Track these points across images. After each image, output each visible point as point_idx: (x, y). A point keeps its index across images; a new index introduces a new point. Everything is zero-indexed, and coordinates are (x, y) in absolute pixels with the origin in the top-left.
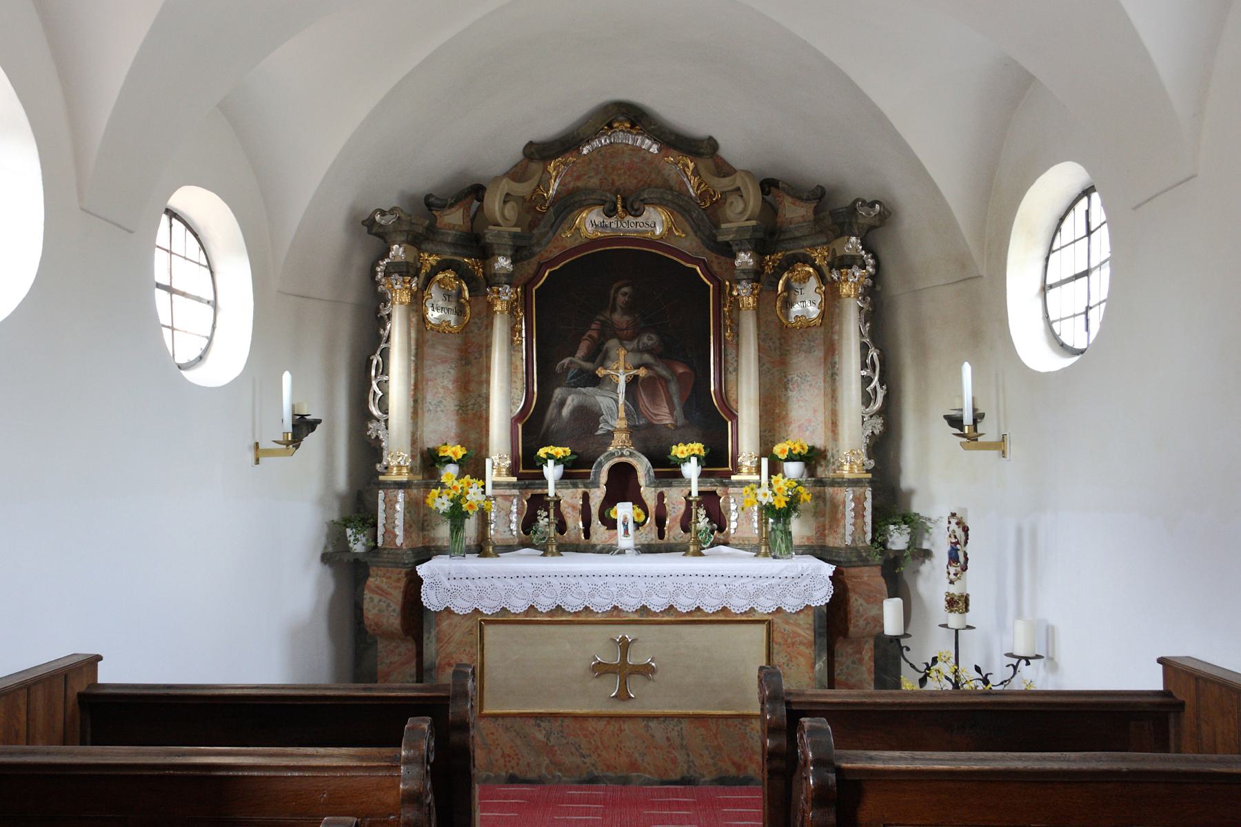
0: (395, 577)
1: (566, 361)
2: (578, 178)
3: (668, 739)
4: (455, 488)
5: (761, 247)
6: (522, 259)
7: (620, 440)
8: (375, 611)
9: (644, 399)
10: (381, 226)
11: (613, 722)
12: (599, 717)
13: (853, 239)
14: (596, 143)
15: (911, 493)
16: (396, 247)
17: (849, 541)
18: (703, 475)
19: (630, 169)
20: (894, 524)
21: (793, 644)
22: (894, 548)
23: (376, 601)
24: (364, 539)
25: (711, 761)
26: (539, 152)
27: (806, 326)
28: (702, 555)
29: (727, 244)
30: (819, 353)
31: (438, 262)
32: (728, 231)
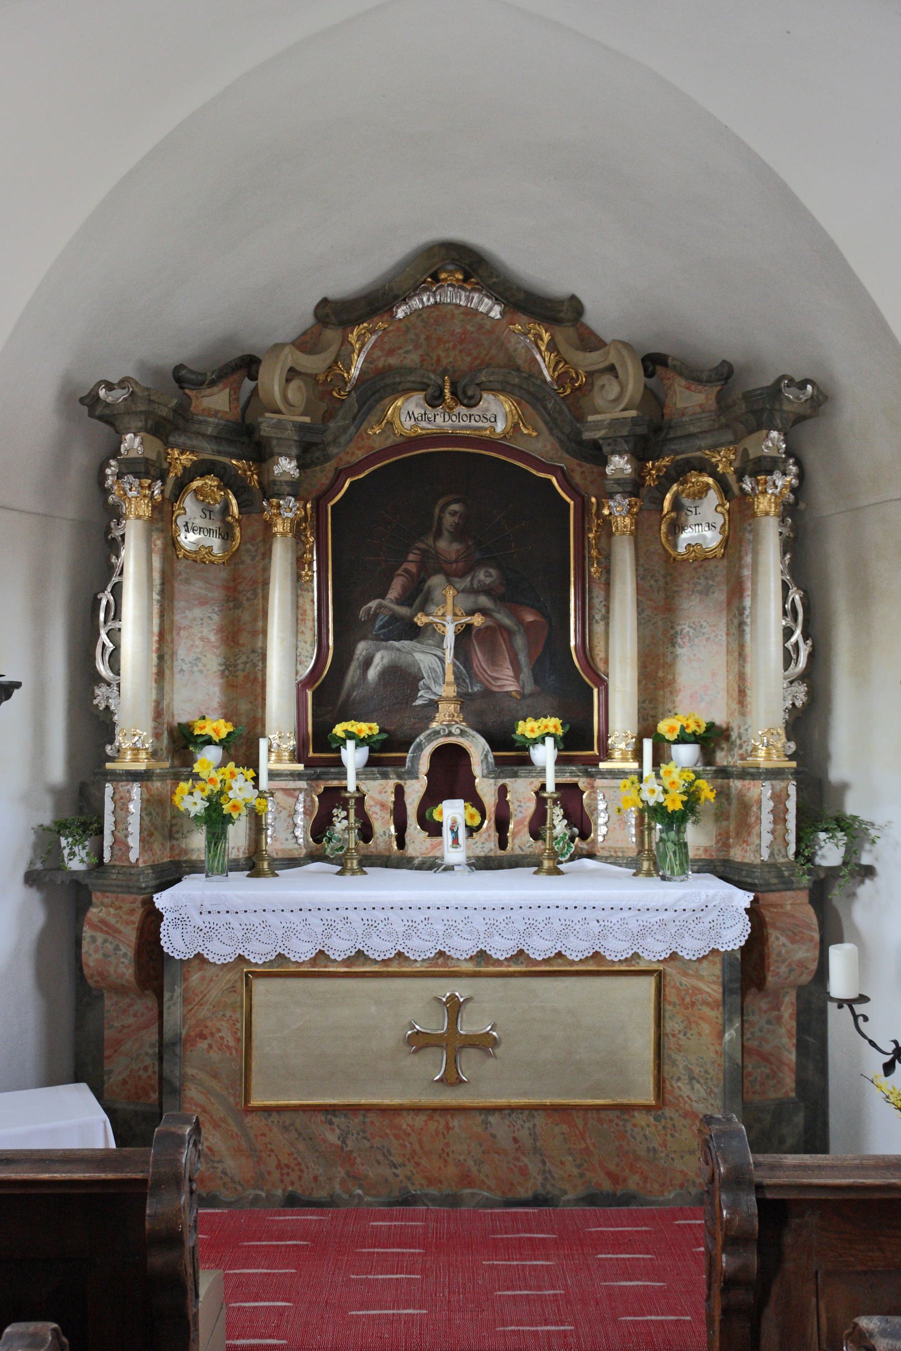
0: (127, 906)
1: (373, 604)
2: (391, 352)
3: (515, 1140)
4: (212, 781)
5: (642, 452)
6: (313, 464)
7: (447, 711)
8: (99, 956)
9: (479, 657)
10: (108, 405)
11: (437, 1117)
12: (417, 1110)
13: (774, 434)
14: (416, 303)
15: (844, 787)
16: (129, 436)
17: (765, 855)
18: (561, 761)
19: (462, 342)
20: (826, 830)
21: (693, 1004)
22: (825, 863)
23: (99, 941)
24: (83, 853)
25: (576, 1171)
26: (337, 314)
27: (701, 558)
28: (559, 873)
29: (596, 445)
30: (720, 596)
31: (194, 463)
32: (598, 425)
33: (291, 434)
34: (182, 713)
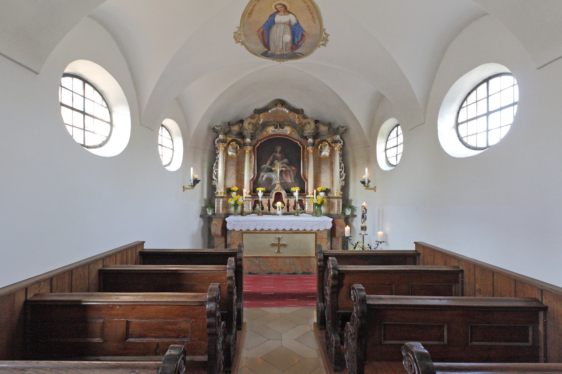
1: (264, 166)
7: (278, 186)
12: (272, 257)
14: (272, 110)
15: (351, 200)
18: (299, 195)
26: (258, 112)
27: (325, 158)
30: (329, 165)
33: (249, 135)
34: (229, 185)
